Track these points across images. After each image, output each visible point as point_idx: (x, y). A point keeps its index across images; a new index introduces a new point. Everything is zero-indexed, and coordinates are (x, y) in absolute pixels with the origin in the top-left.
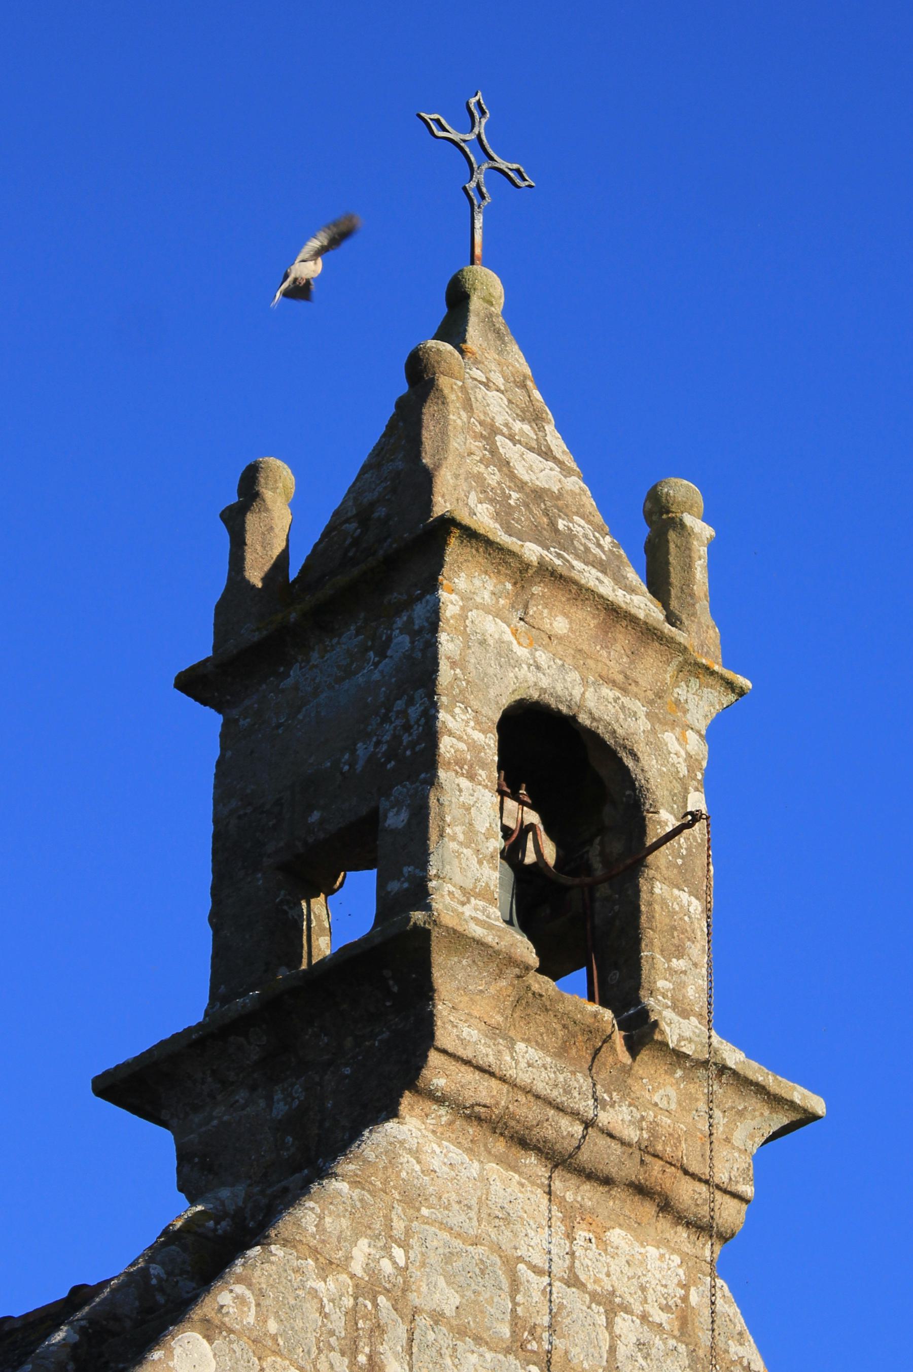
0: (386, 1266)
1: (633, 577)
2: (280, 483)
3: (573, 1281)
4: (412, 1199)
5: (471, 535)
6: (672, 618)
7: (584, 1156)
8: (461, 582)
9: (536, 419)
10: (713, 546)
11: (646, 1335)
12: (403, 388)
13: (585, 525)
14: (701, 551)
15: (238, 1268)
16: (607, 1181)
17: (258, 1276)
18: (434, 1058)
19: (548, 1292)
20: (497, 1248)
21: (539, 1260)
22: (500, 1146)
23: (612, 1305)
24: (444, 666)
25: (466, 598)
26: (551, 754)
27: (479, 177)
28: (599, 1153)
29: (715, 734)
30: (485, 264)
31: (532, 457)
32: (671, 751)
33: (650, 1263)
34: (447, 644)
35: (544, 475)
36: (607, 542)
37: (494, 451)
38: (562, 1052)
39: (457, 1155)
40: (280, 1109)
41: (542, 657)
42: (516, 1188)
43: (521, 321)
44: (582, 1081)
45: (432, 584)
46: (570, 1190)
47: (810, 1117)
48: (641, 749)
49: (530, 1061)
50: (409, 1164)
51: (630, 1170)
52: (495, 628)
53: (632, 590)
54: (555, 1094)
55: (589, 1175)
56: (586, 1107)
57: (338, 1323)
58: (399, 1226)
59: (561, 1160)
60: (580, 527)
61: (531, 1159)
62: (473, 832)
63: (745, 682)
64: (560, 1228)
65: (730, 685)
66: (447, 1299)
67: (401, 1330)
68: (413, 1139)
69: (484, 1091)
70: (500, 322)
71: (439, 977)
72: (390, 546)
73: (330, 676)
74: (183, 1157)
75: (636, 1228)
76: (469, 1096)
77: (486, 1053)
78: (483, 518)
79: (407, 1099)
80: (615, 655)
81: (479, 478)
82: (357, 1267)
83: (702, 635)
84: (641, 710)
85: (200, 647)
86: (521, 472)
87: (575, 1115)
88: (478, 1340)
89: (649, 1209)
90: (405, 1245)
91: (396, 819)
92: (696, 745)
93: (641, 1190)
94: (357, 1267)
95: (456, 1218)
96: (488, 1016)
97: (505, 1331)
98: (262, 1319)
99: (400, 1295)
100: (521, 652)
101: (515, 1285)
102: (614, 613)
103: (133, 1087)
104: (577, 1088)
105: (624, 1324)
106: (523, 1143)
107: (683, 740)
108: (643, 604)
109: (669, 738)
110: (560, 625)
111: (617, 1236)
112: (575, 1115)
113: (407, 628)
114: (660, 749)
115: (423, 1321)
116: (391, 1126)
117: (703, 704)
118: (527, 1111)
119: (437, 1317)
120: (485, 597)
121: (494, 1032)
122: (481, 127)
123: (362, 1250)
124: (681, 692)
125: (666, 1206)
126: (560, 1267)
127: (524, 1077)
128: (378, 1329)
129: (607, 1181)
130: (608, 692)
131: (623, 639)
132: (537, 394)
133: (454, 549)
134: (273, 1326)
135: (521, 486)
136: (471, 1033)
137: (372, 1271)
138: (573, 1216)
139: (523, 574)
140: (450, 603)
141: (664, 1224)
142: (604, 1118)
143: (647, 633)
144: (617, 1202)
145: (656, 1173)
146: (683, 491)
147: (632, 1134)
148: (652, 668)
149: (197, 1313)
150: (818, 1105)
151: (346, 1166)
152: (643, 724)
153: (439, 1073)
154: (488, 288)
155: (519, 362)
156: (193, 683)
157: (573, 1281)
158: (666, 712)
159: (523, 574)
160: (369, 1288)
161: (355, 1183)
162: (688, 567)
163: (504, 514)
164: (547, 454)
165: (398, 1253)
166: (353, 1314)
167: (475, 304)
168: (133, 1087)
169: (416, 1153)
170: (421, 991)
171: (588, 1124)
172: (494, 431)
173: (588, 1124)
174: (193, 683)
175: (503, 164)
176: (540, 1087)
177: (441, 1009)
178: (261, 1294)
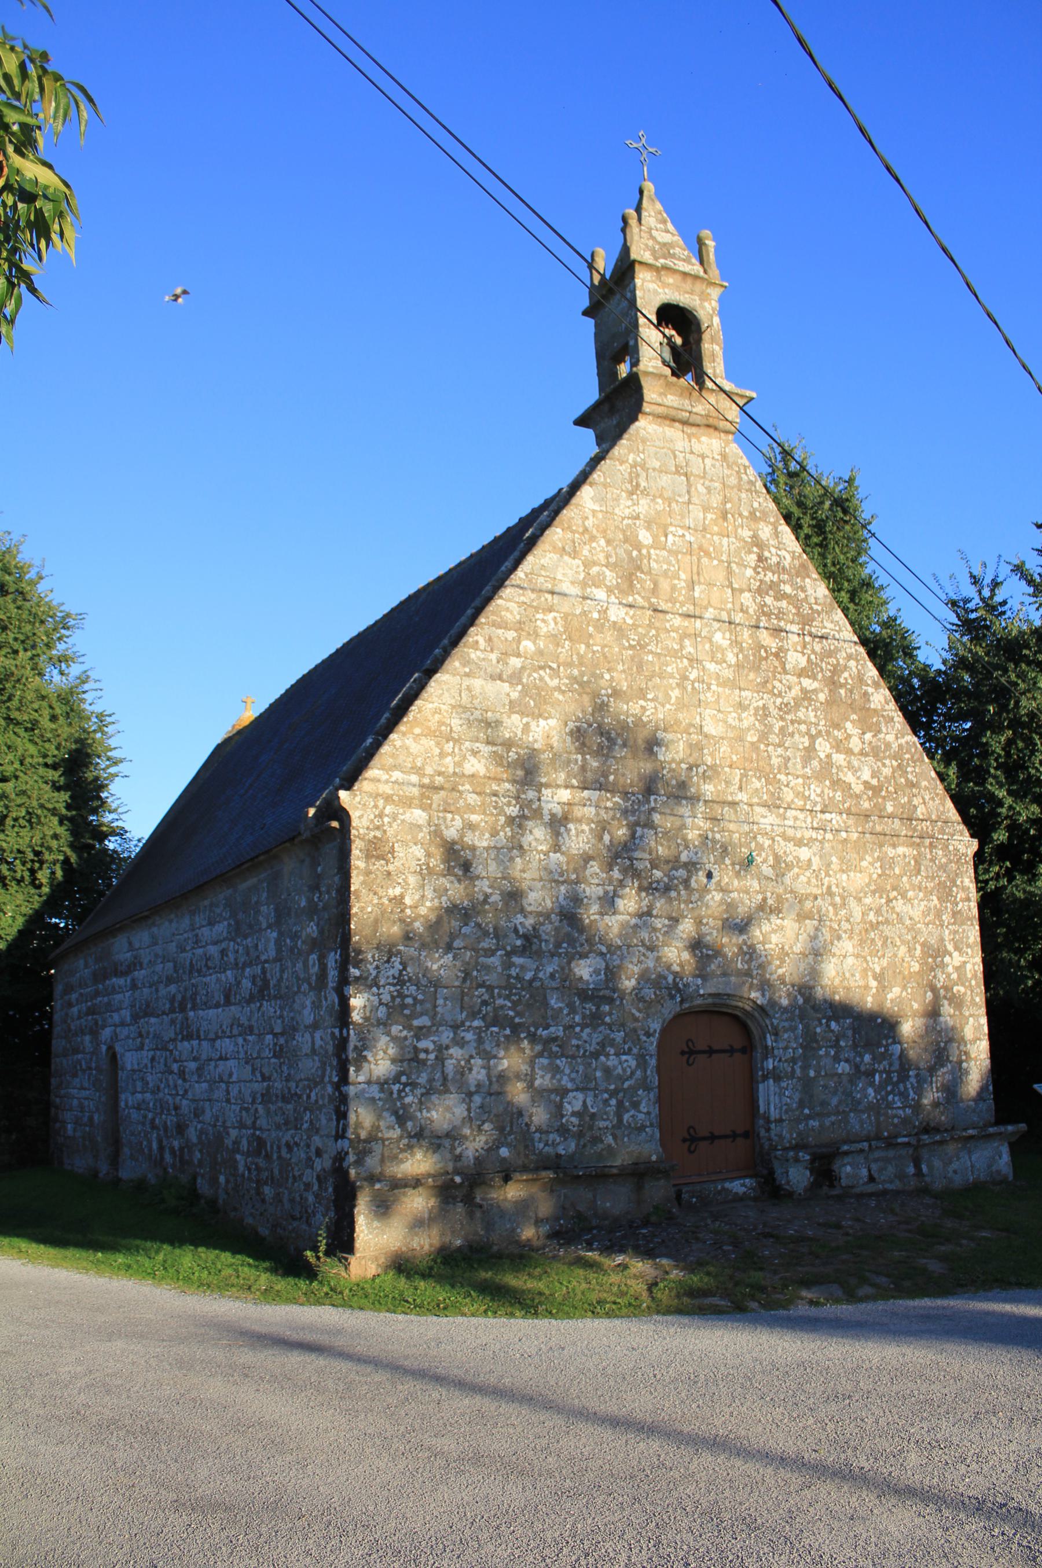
0: (638, 459)
1: (694, 261)
2: (601, 252)
3: (692, 452)
4: (644, 441)
5: (641, 263)
6: (705, 272)
7: (691, 421)
8: (641, 276)
9: (664, 222)
10: (716, 248)
11: (714, 462)
12: (622, 224)
13: (681, 251)
14: (712, 251)
15: (599, 467)
16: (698, 426)
17: (603, 469)
18: (645, 404)
19: (685, 457)
20: (669, 449)
21: (681, 449)
22: (668, 422)
23: (703, 457)
24: (638, 300)
25: (644, 280)
26: (673, 316)
27: (644, 156)
28: (694, 419)
29: (721, 300)
30: (649, 180)
31: (664, 234)
32: (707, 308)
33: (711, 444)
34: (638, 293)
35: (667, 238)
36: (686, 253)
37: (651, 235)
38: (681, 395)
39: (655, 427)
40: (615, 422)
41: (666, 290)
42: (674, 433)
43: (659, 195)
44: (687, 401)
45: (633, 278)
46: (688, 430)
47: (752, 399)
48: (698, 309)
49: (672, 400)
50: (642, 433)
51: (704, 421)
52: (652, 286)
53: (693, 265)
54: (680, 407)
55: (693, 425)
56: (689, 408)
57: (627, 476)
58: (641, 448)
59: (685, 423)
60: (677, 250)
61: (677, 424)
62: (653, 343)
63: (726, 284)
64: (687, 440)
65: (722, 286)
66: (657, 464)
67: (645, 474)
68: (643, 426)
69: (660, 410)
70: (653, 197)
71: (643, 383)
72: (625, 269)
73: (615, 306)
74: (597, 437)
75: (709, 436)
76: (656, 412)
77: (659, 401)
78: (647, 257)
79: (640, 416)
80: (688, 285)
81: (646, 245)
82: (630, 461)
83: (715, 273)
84: (697, 298)
85: (586, 303)
86: (660, 239)
87: (686, 411)
88: (666, 473)
89: (712, 430)
90: (643, 453)
91: (632, 343)
92: (715, 304)
93: (708, 426)
94: (630, 461)
95: (657, 443)
96: (659, 390)
97: (674, 469)
98: (605, 479)
99: (643, 466)
100: (660, 291)
101: (675, 457)
102: (685, 274)
103: (582, 421)
104: (686, 403)
105: (707, 461)
106: (674, 420)
107: (710, 304)
108: (696, 268)
109: (706, 304)
110: (671, 281)
111: (704, 439)
112: (686, 411)
113: (688, 256)
114: (704, 308)
115: (650, 471)
116: (637, 424)
117: (715, 293)
118: (673, 413)
119: (654, 469)
120: (649, 278)
121: (661, 394)
122: (643, 140)
123: (631, 457)
124: (709, 291)
125: (716, 429)
126: (688, 450)
127: (670, 404)
128: (638, 475)
129: (698, 426)
130: (687, 296)
131: (689, 281)
132: (665, 215)
133: (637, 267)
134: (608, 480)
135: (659, 243)
136: (654, 396)
137: (635, 461)
138: (689, 436)
139: (658, 270)
140: (638, 282)
141: (717, 433)
142: (694, 410)
143: (696, 277)
144: (702, 430)
145: (711, 421)
146: (706, 233)
147: (703, 413)
148: (699, 286)
149: (588, 481)
150: (754, 395)
151: (626, 436)
152: (698, 302)
153: (646, 408)
154: (649, 187)
155: (659, 206)
156: (586, 313)
157: (692, 452)
158: (704, 297)
159: (658, 270)
160: (634, 465)
161: (628, 440)
162: (708, 255)
163: (654, 253)
164: (667, 231)
165: (642, 456)
166: (630, 473)
167: (645, 193)
168: (582, 421)
169: (644, 429)
170: (639, 388)
171: (690, 412)
172: (651, 229)
173: (690, 412)
174: (586, 313)
175: (651, 150)
176: (675, 405)
177: (645, 391)
178: (604, 473)
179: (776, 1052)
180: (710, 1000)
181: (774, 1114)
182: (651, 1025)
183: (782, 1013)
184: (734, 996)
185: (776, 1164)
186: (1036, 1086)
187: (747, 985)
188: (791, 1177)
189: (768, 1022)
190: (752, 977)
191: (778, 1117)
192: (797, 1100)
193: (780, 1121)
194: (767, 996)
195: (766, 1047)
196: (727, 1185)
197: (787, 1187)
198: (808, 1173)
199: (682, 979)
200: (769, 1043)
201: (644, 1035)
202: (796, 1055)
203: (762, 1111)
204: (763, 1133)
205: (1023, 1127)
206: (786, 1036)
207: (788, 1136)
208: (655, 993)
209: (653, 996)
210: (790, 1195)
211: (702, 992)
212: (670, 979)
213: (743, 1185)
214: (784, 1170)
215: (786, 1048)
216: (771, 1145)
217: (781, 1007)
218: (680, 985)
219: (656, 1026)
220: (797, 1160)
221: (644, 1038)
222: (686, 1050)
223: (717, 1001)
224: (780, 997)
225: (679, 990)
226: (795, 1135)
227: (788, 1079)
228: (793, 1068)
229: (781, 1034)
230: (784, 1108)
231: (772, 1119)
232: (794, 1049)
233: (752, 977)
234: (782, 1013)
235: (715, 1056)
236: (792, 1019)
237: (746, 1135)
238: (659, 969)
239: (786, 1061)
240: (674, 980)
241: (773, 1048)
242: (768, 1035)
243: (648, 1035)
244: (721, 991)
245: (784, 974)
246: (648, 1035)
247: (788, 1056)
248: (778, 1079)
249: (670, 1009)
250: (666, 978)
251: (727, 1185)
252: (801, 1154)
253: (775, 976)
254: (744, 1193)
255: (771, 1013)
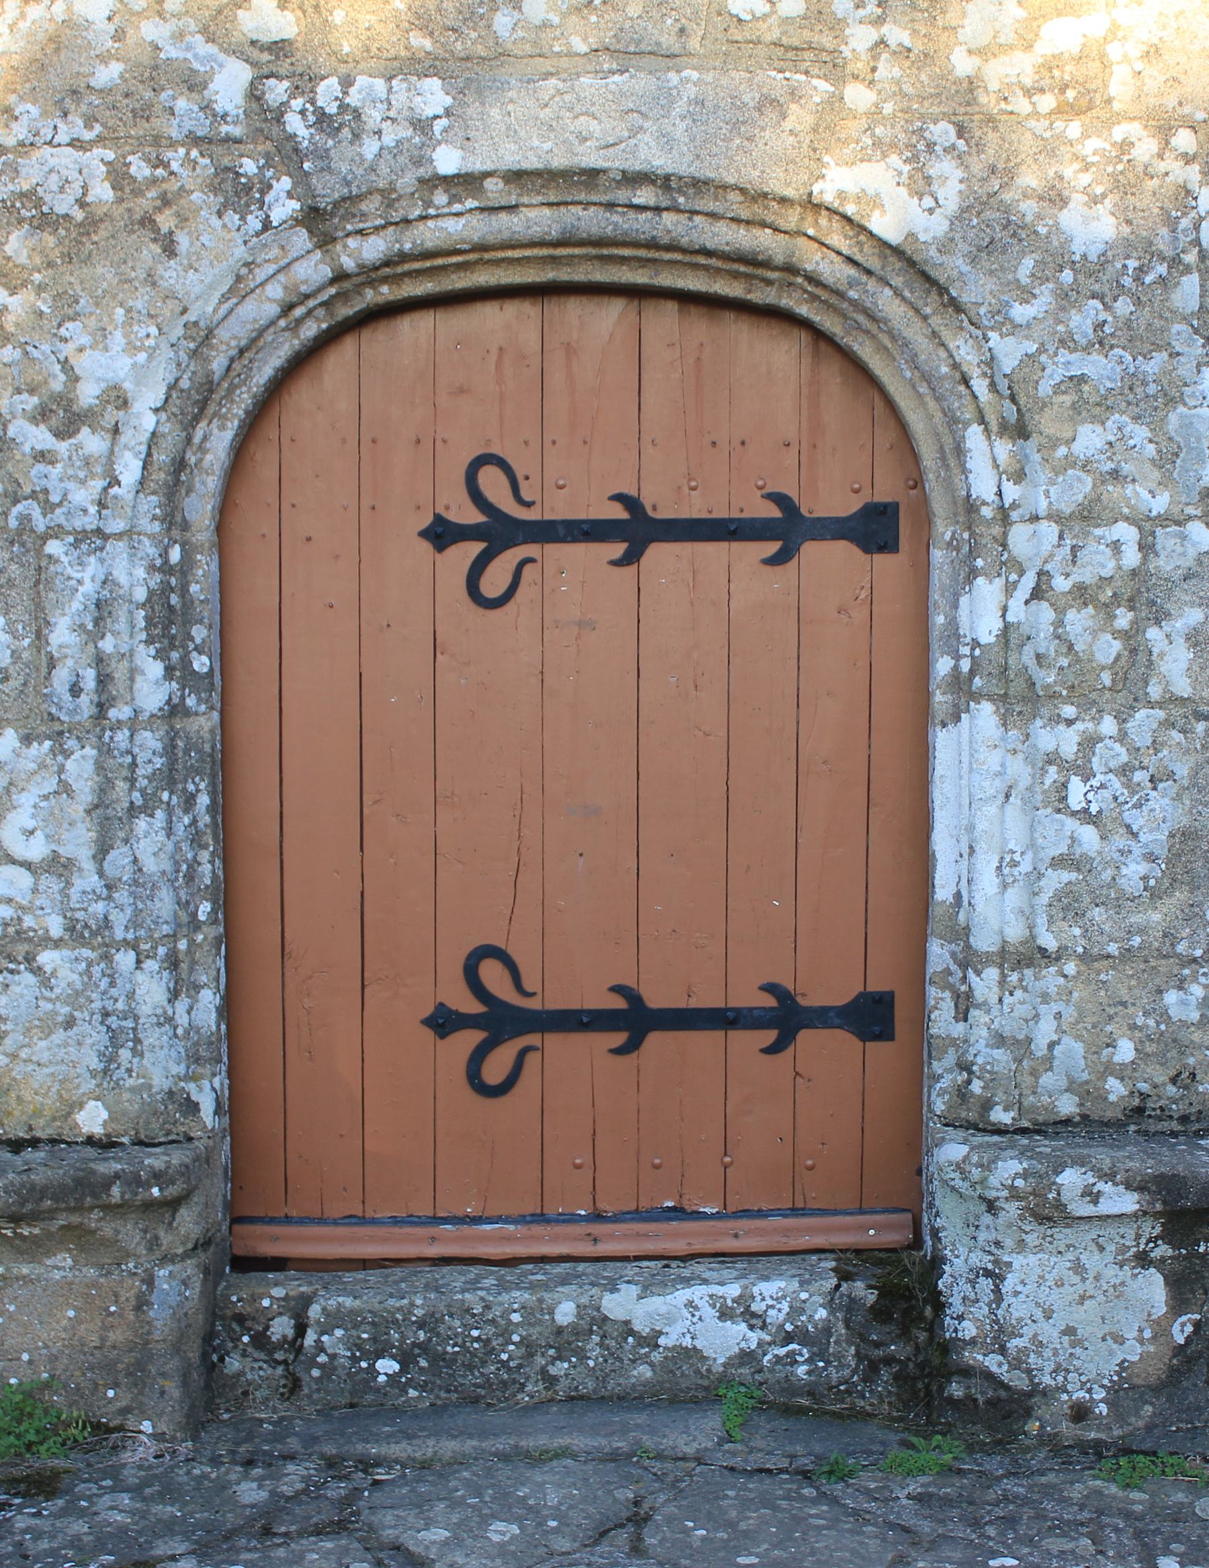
179: (1019, 537)
180: (536, 219)
181: (996, 915)
182: (84, 364)
183: (1067, 299)
184: (699, 185)
185: (948, 1216)
186: (625, 545)
187: (799, 117)
188: (1017, 1309)
189: (966, 353)
190: (834, 67)
191: (1015, 932)
192: (1155, 838)
193: (1027, 957)
194: (950, 194)
195: (970, 507)
196: (624, 1304)
197: (993, 1363)
198: (1153, 1290)
199: (305, 82)
200: (983, 485)
201: (41, 415)
202: (1164, 564)
203: (943, 892)
204: (942, 1020)
205: (741, 1560)
206: (1089, 439)
207: (1073, 1051)
208: (118, 176)
209: (102, 192)
210: (1006, 1410)
211: (447, 161)
212: (230, 84)
213: (743, 1311)
214: (979, 1259)
215: (1088, 515)
216: (962, 1093)
217: (1057, 258)
218: (294, 124)
219: (126, 364)
220: (1048, 1213)
221: (40, 437)
222: (467, 515)
223: (591, 221)
224: (1056, 198)
225: (288, 154)
226: (1125, 1051)
227: (1089, 705)
228: (1132, 638)
229: (1046, 424)
230: (1056, 879)
231: (984, 942)
232: (1149, 528)
233: (834, 67)
234: (1067, 299)
235: (659, 555)
236: (1143, 339)
237: (872, 1016)
238: (151, 30)
239: (1082, 594)
240: (254, 95)
241: (1004, 515)
242: (974, 436)
243: (65, 416)
244: (590, 158)
245: (1094, 55)
246: (65, 416)
247: (1097, 563)
248: (1022, 701)
249: (234, 268)
250: (194, 83)
251: (624, 1304)
252: (1071, 1179)
253: (1019, 66)
254: (746, 1357)
255: (976, 290)
